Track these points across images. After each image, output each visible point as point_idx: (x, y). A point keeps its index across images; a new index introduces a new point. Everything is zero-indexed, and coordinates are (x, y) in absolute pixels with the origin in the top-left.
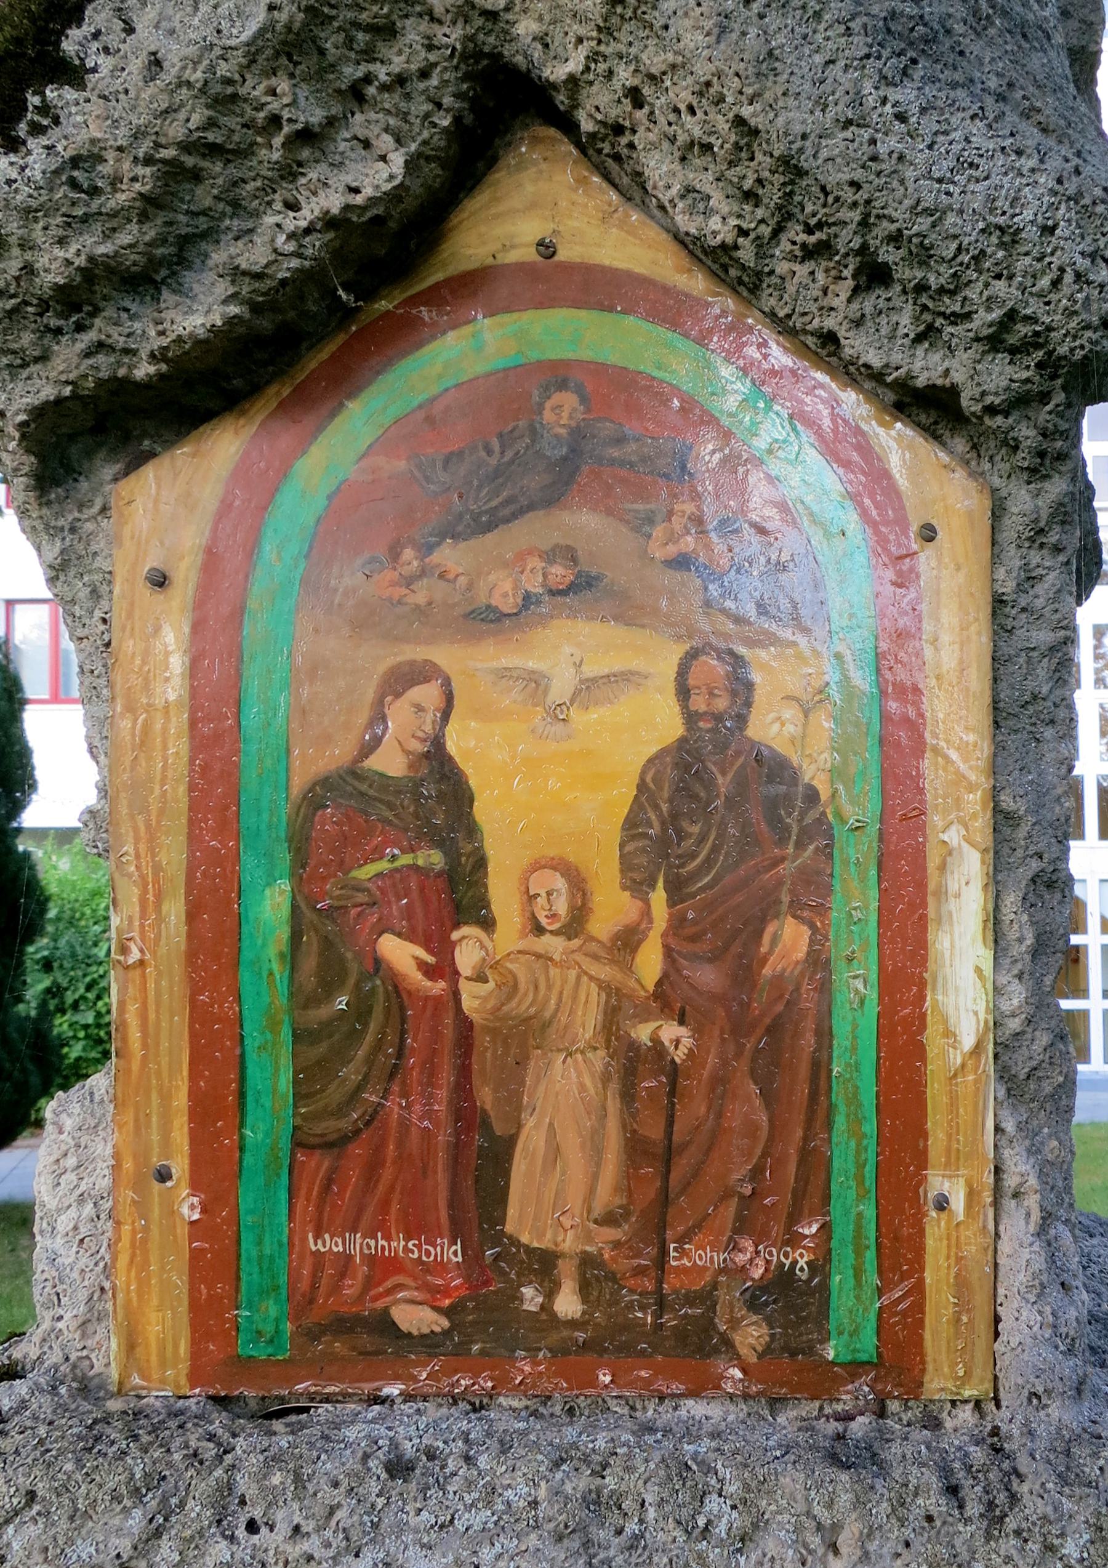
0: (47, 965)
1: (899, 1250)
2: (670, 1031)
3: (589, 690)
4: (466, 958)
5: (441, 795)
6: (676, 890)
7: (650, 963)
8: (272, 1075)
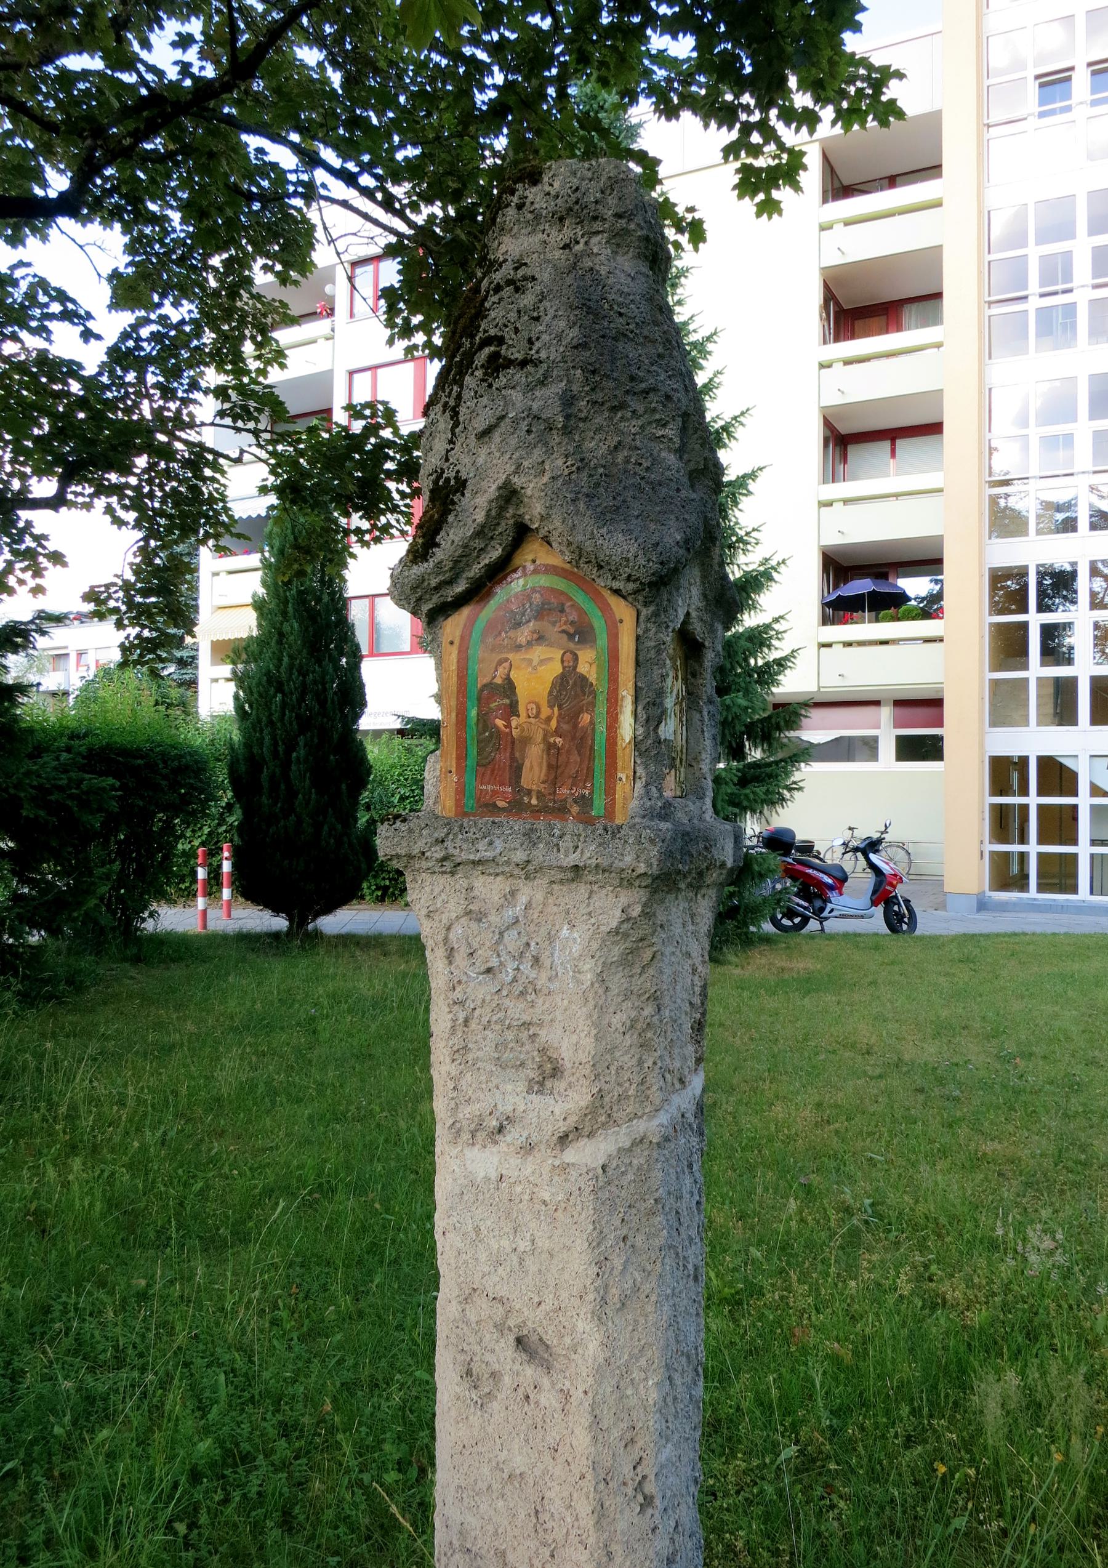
0: (368, 807)
1: (610, 791)
2: (558, 740)
3: (542, 662)
4: (514, 723)
5: (509, 687)
6: (560, 707)
7: (554, 724)
8: (473, 750)
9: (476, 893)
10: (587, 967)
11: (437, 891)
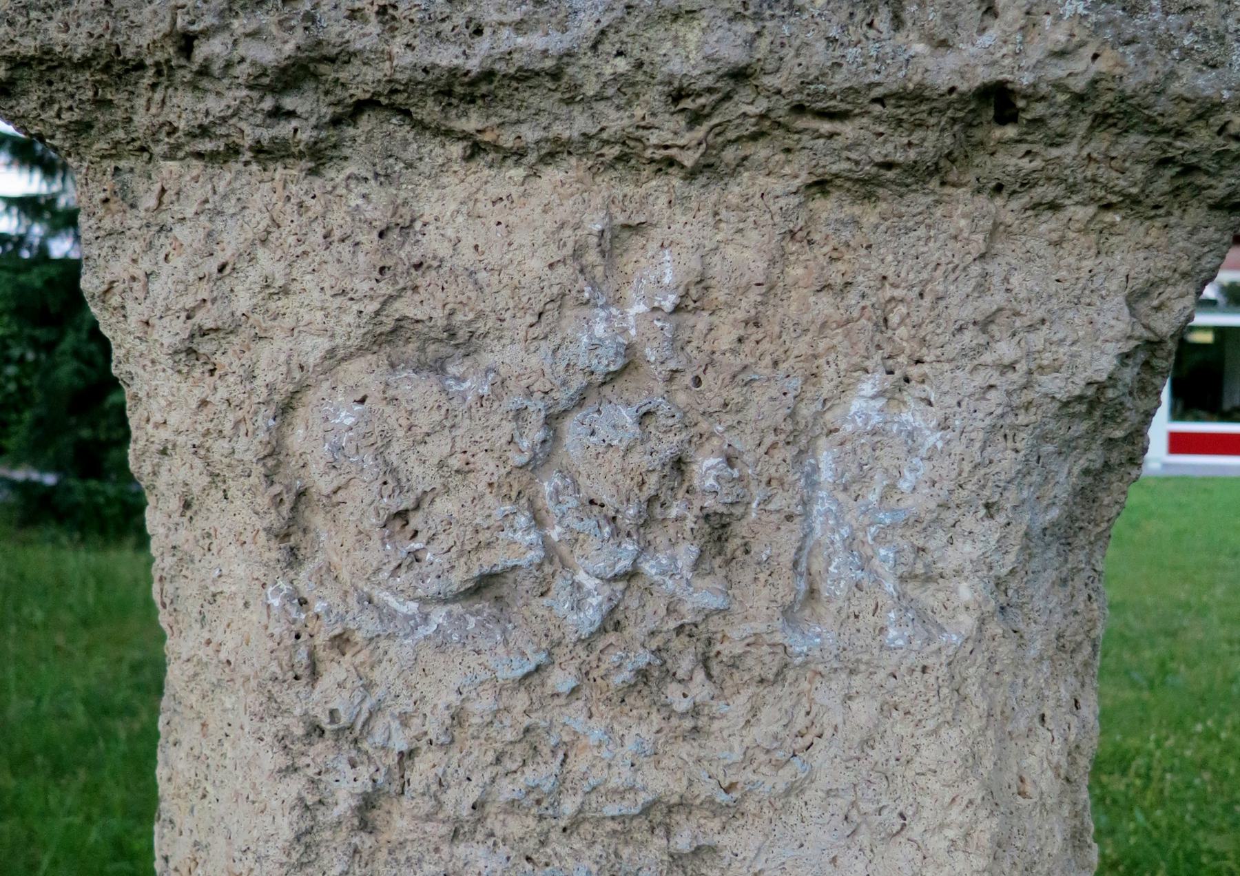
9: (432, 244)
10: (966, 550)
11: (232, 241)
